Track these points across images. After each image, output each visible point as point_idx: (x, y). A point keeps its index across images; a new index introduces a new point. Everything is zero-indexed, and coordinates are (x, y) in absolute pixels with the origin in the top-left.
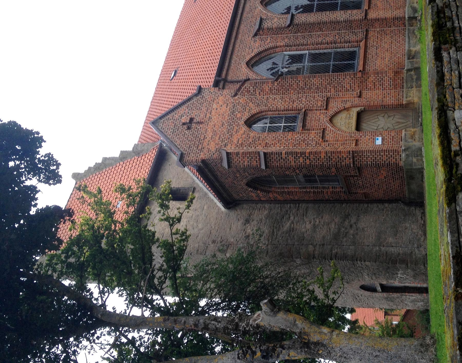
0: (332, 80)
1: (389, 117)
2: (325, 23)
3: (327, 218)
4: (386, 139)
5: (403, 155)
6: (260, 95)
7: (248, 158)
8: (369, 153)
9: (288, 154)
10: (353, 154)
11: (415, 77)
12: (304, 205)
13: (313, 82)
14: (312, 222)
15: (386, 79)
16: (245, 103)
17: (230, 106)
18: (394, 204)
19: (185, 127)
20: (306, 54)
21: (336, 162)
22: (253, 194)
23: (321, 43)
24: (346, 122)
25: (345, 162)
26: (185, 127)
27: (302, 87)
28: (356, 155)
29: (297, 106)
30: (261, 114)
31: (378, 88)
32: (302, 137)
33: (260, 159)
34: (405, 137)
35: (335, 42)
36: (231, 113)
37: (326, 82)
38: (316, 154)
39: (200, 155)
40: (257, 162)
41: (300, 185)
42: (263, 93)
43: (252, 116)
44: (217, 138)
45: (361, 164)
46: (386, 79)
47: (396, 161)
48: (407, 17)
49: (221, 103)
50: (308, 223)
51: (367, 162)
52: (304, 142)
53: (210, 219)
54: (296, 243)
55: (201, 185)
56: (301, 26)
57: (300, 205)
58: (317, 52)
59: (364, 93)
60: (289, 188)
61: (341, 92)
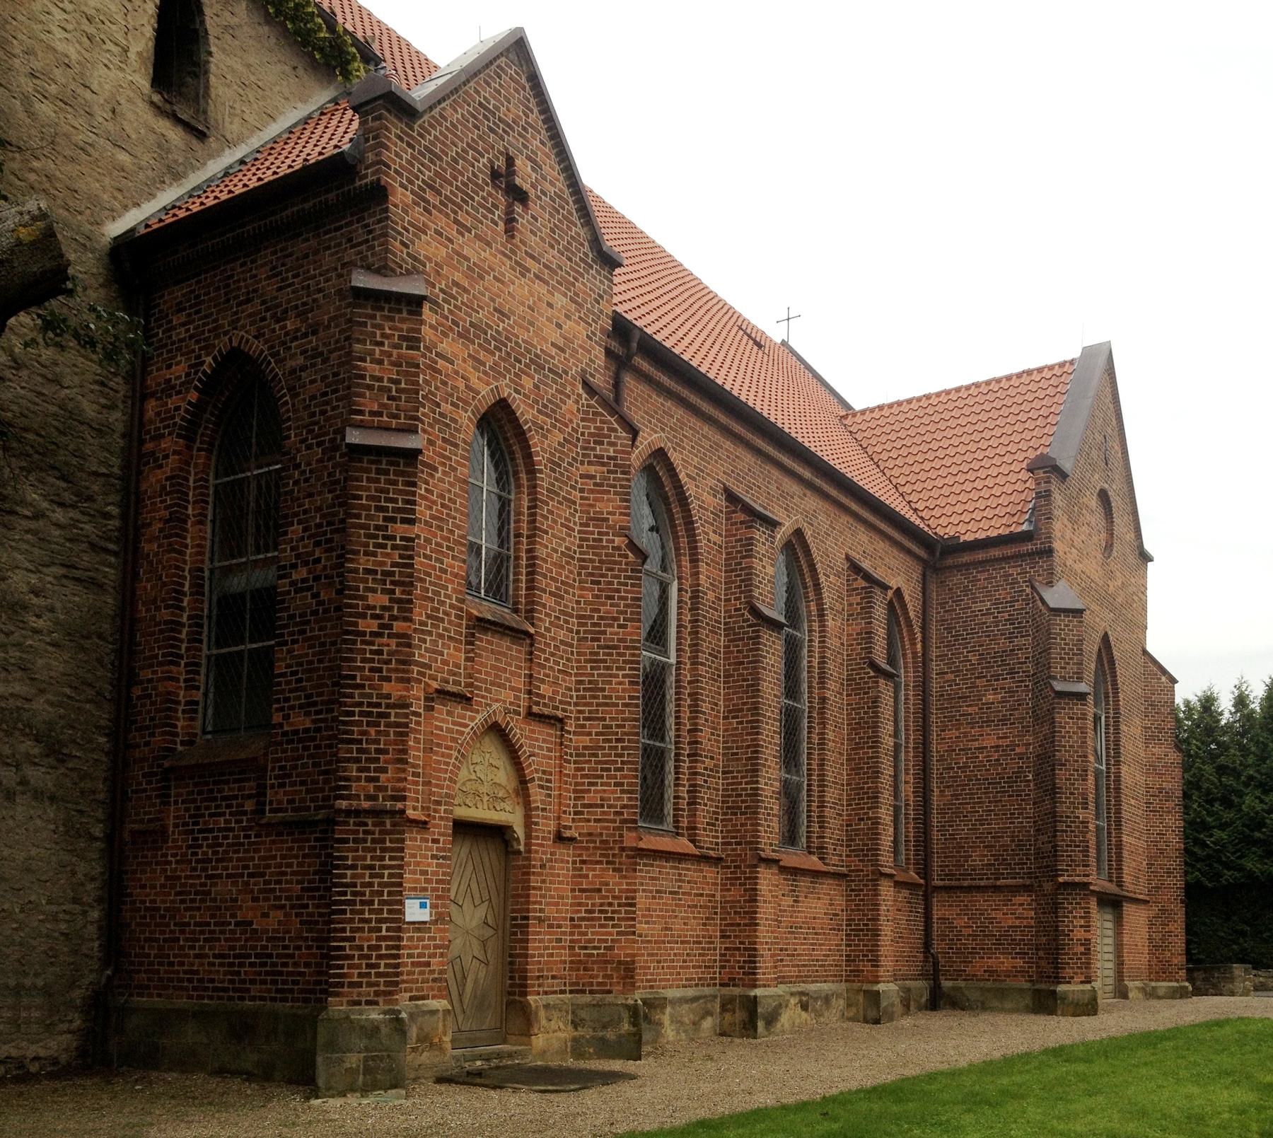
0: (618, 740)
1: (484, 943)
2: (755, 729)
3: (53, 664)
4: (420, 939)
5: (375, 1015)
6: (582, 476)
7: (391, 380)
8: (391, 876)
9: (406, 548)
10: (392, 813)
11: (610, 1035)
12: (110, 574)
13: (617, 676)
14: (35, 600)
15: (610, 934)
16: (563, 416)
17: (557, 361)
18: (96, 944)
19: (501, 163)
20: (665, 653)
21: (360, 742)
22: (179, 370)
23: (695, 709)
24: (478, 785)
25: (358, 779)
26: (501, 163)
27: (604, 633)
28: (388, 822)
30: (522, 468)
31: (580, 904)
32: (445, 613)
33: (387, 429)
34: (425, 1013)
35: (695, 755)
36: (536, 355)
37: (612, 719)
38: (399, 662)
39: (402, 185)
40: (372, 413)
41: (212, 571)
42: (591, 491)
43: (521, 435)
44: (458, 276)
45: (346, 841)
46: (610, 934)
47: (351, 985)
48: (758, 992)
49: (568, 325)
50: (34, 579)
51: (354, 867)
52: (428, 617)
53: (73, 160)
55: (215, 167)
56: (751, 650)
57: (113, 559)
58: (671, 693)
59: (567, 854)
60: (201, 523)
61: (577, 769)
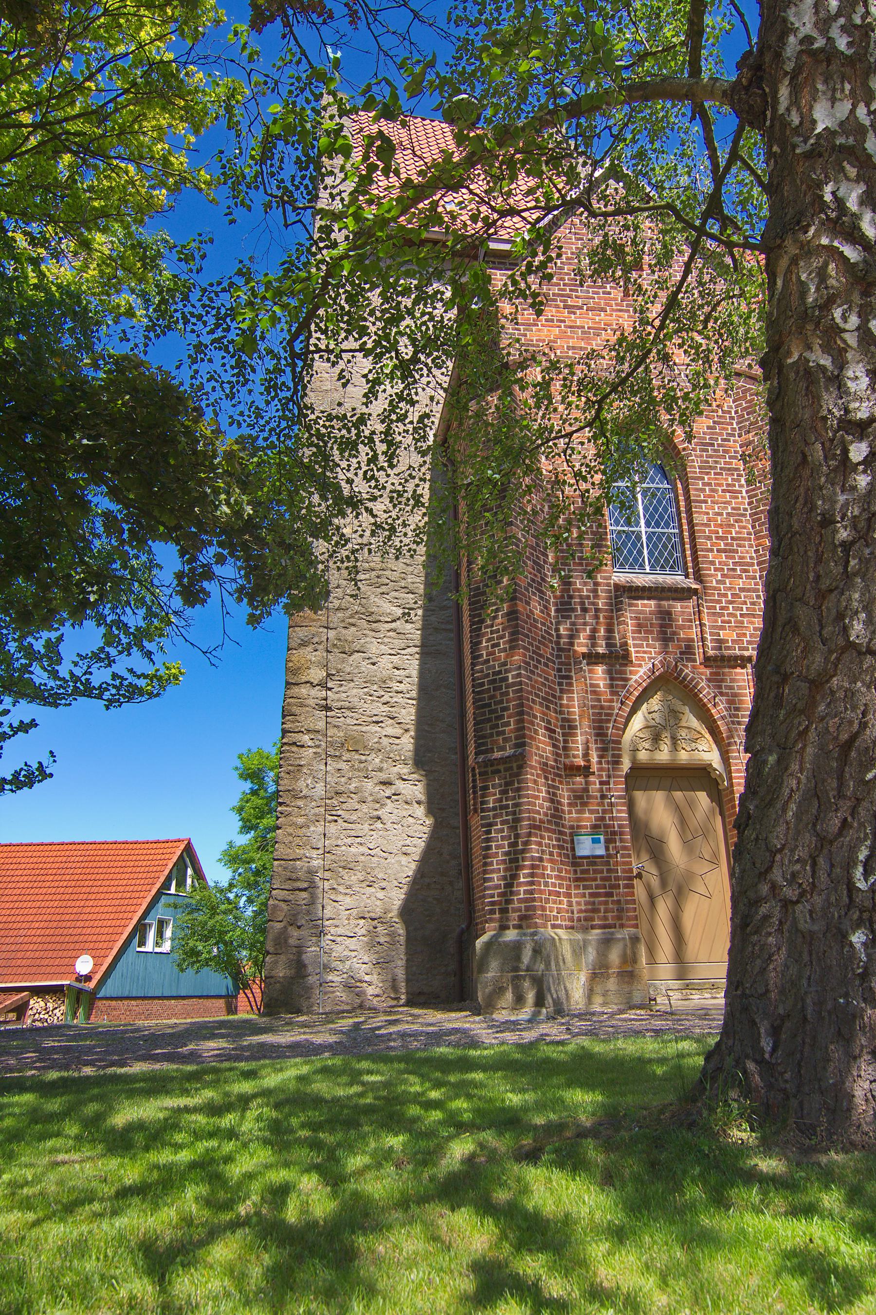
29: (712, 563)
54: (332, 634)
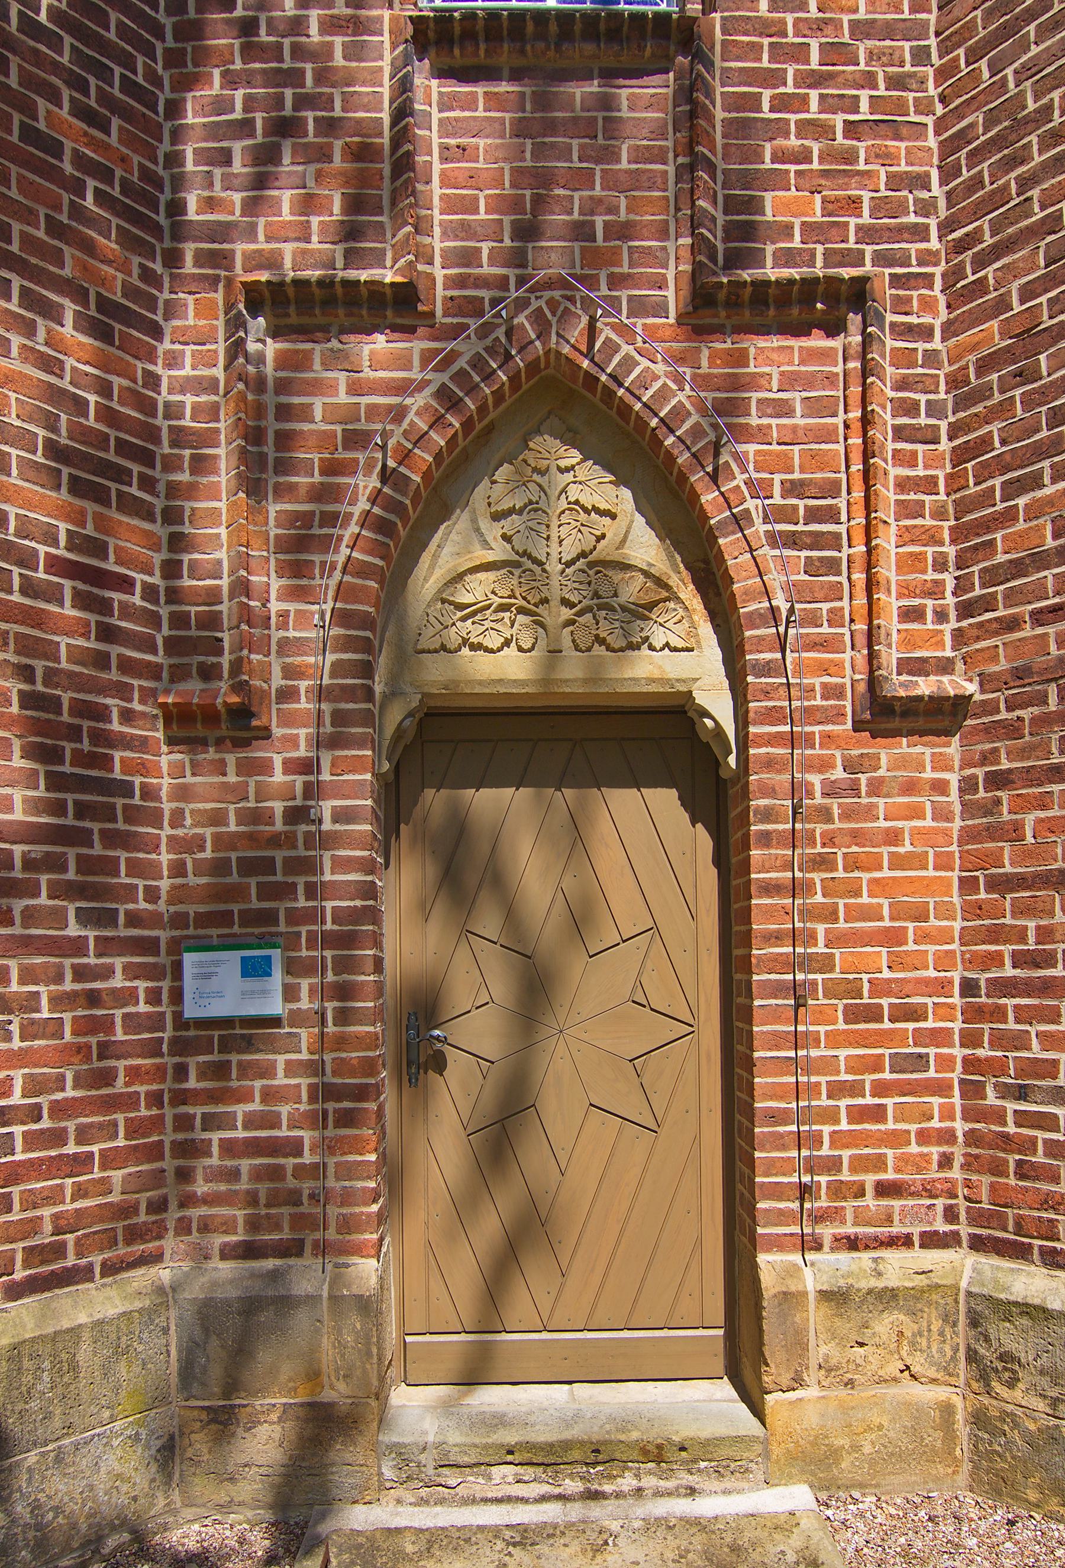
31: (995, 935)
